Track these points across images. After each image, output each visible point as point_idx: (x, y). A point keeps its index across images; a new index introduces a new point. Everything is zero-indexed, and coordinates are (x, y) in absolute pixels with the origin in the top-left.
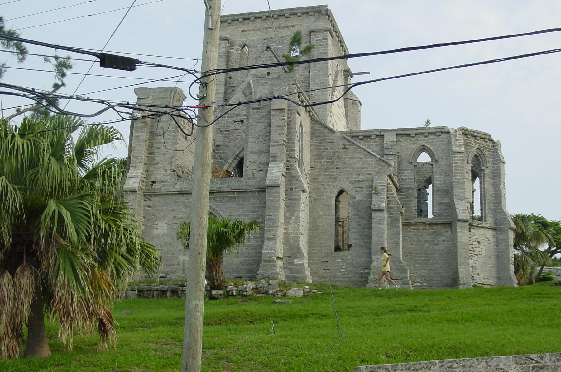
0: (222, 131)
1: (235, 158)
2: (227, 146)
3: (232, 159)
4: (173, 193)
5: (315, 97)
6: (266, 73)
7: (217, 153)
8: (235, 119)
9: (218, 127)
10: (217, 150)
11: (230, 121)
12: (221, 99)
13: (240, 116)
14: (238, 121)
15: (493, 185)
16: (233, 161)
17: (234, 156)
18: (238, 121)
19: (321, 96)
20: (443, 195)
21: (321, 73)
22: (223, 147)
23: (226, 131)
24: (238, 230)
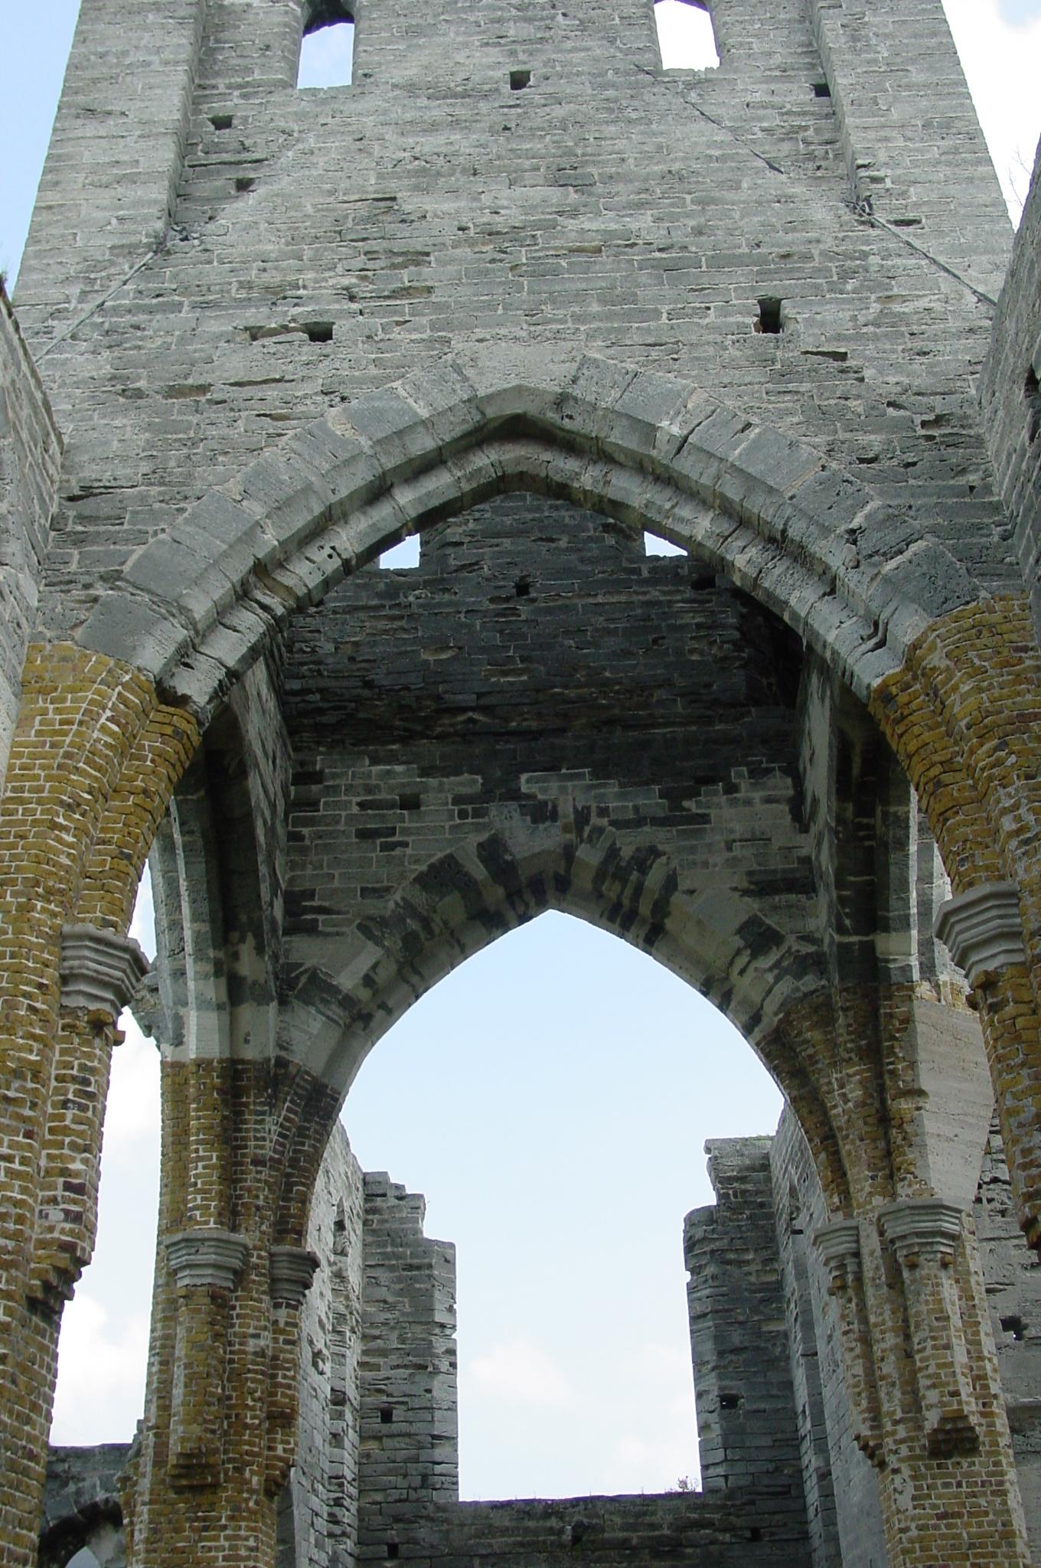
0: (139, 394)
1: (242, 595)
2: (178, 492)
3: (219, 589)
4: (101, 947)
5: (904, 194)
6: (502, 74)
7: (80, 540)
8: (256, 316)
9: (108, 370)
10: (82, 519)
11: (215, 325)
12: (154, 211)
13: (299, 301)
14: (286, 329)
15: (503, 478)
16: (220, 618)
17: (239, 568)
18: (286, 329)
19: (953, 189)
20: (475, 669)
21: (916, 76)
22: (143, 498)
23: (173, 392)
24: (287, 1324)
